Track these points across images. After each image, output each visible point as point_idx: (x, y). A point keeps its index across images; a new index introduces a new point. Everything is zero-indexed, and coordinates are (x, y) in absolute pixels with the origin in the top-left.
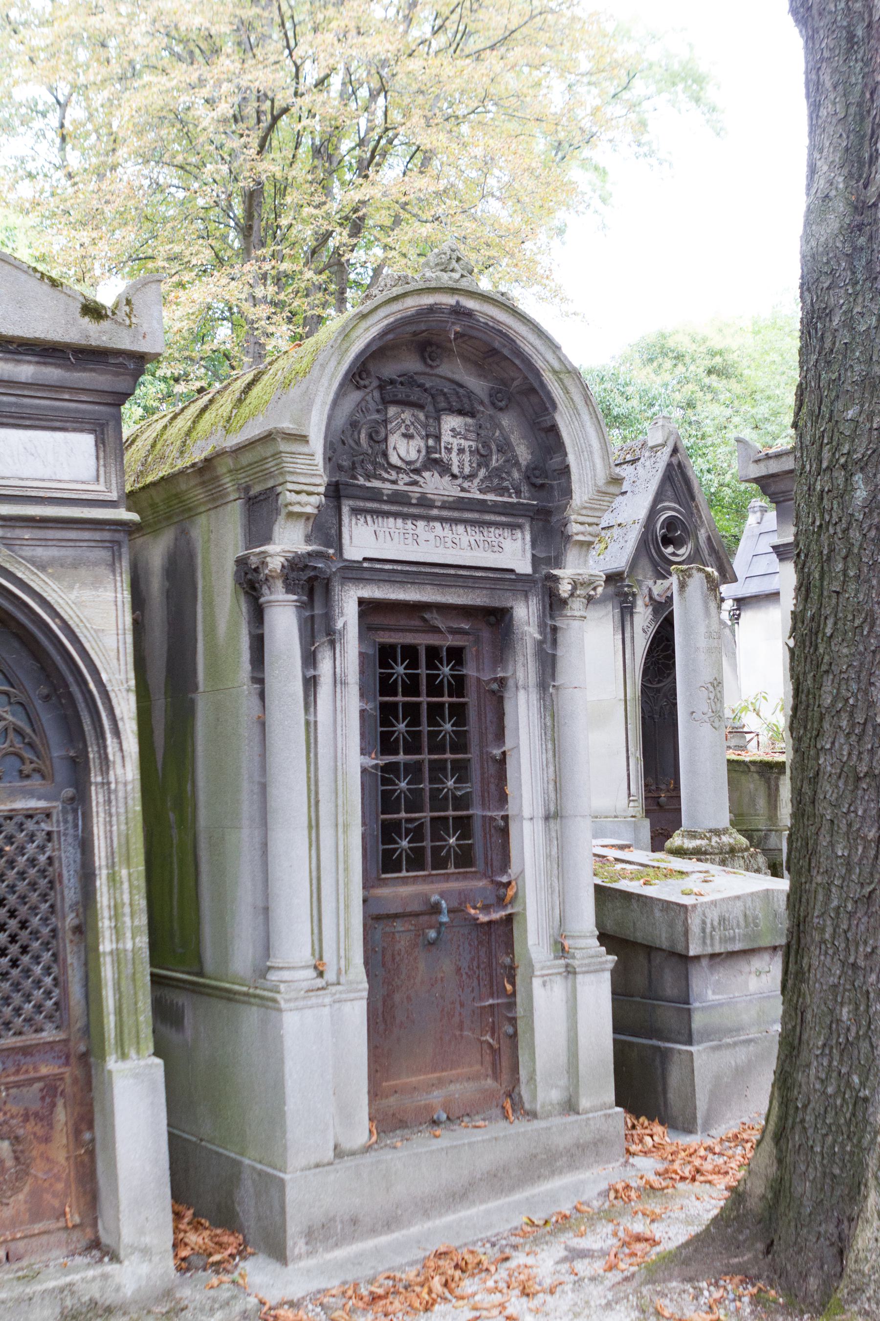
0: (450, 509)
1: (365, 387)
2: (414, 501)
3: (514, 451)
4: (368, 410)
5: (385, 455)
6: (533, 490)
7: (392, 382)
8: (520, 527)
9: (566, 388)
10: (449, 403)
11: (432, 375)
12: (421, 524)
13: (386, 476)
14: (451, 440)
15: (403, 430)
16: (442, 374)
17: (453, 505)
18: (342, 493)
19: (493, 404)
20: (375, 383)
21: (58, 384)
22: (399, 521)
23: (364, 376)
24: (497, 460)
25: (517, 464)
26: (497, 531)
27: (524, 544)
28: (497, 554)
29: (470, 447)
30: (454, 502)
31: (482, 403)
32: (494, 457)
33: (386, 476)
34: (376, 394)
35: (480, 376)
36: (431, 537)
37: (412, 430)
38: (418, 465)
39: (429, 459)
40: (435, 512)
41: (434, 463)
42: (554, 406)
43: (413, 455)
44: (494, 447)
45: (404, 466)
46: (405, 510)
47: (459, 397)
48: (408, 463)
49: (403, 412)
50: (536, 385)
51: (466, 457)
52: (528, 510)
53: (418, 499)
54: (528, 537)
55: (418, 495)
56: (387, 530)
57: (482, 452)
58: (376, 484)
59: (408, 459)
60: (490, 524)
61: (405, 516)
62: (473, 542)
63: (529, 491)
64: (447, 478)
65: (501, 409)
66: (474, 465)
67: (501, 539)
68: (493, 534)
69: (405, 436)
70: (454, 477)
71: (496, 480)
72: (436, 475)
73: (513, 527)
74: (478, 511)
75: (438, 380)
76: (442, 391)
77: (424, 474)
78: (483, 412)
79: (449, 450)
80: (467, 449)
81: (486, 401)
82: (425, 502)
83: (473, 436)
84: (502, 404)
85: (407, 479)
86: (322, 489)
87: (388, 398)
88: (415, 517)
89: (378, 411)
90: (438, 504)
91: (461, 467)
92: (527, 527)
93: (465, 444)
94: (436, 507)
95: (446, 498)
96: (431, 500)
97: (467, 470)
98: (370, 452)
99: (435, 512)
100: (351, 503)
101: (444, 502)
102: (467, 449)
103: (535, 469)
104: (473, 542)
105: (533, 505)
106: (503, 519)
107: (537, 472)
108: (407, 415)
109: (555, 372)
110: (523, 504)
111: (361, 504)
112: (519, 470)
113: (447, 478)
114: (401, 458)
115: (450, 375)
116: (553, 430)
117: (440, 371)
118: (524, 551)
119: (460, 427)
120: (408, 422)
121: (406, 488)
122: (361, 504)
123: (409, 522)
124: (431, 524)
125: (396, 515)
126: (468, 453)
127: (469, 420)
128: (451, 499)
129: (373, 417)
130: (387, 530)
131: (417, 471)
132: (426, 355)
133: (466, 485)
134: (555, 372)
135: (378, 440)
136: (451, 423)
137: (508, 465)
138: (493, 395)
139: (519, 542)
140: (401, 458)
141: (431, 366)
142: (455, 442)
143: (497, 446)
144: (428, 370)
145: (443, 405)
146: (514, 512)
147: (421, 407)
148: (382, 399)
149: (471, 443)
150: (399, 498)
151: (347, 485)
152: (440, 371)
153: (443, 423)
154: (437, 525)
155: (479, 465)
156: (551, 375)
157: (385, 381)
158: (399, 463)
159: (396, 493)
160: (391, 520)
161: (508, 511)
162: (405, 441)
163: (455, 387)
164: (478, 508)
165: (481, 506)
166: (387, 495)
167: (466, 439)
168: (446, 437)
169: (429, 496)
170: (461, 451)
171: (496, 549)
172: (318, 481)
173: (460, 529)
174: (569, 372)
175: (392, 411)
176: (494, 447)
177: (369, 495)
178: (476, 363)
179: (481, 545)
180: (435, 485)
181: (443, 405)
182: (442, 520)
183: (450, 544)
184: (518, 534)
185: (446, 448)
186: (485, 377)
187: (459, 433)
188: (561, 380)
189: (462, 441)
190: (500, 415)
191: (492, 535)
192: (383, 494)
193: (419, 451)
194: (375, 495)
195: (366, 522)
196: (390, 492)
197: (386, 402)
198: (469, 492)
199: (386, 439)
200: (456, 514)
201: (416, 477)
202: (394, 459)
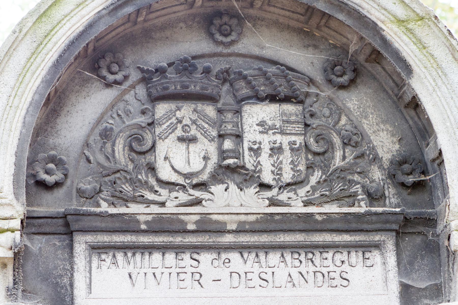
0: (253, 231)
1: (116, 83)
2: (191, 227)
3: (370, 142)
4: (128, 113)
5: (152, 169)
6: (405, 193)
7: (160, 71)
8: (377, 246)
9: (420, 41)
10: (253, 88)
11: (230, 55)
12: (206, 258)
13: (150, 196)
14: (259, 138)
15: (179, 132)
16: (243, 51)
17: (257, 227)
18: (74, 226)
19: (330, 81)
20: (135, 76)
21: (311, 233)
22: (170, 257)
23: (115, 68)
24: (344, 158)
25: (376, 159)
26: (338, 257)
27: (386, 271)
28: (339, 290)
29: (292, 143)
30: (257, 221)
31: (311, 82)
32: (338, 154)
33: (150, 196)
34: (141, 91)
35: (307, 47)
36: (224, 273)
37: (193, 131)
38: (205, 177)
39: (220, 166)
40: (228, 239)
41: (231, 171)
42: (408, 69)
43: (197, 164)
44: (337, 141)
45: (181, 181)
46: (178, 240)
47: (268, 79)
48: (187, 176)
49: (179, 109)
50: (377, 45)
51: (287, 157)
52: (387, 222)
53: (196, 222)
54: (392, 260)
55: (197, 218)
56: (151, 271)
57: (315, 147)
58: (134, 208)
59: (186, 170)
60: (324, 247)
61: (179, 249)
62: (296, 276)
63: (398, 194)
64: (252, 190)
65: (342, 87)
66: (302, 167)
67: (345, 267)
68: (330, 262)
69: (181, 139)
70: (264, 186)
71: (337, 185)
72: (233, 187)
73: (365, 248)
74: (301, 231)
75: (240, 61)
76: (240, 73)
77: (213, 189)
78: (317, 95)
79: (256, 152)
80: (286, 147)
81: (319, 78)
82: (207, 226)
83: (299, 128)
84: (344, 79)
85: (183, 197)
86: (16, 224)
87: (155, 93)
88: (196, 249)
89: (143, 112)
90: (234, 227)
91: (278, 171)
92: (390, 245)
93: (285, 140)
94: (229, 232)
95: (243, 218)
96: (217, 222)
97: (287, 177)
98: (131, 167)
99: (228, 239)
100: (90, 238)
101: (241, 223)
102: (286, 147)
103: (402, 163)
104: (296, 276)
105: (395, 214)
106: (347, 238)
107: (406, 167)
108: (186, 111)
109: (401, 22)
110: (376, 214)
111: (105, 238)
112: (381, 167)
113: (252, 190)
114: (176, 171)
115: (256, 51)
116: (415, 104)
117: (239, 48)
118: (386, 281)
119: (274, 119)
120: (187, 121)
121: (175, 210)
122: (105, 238)
123: (187, 256)
124: (224, 256)
125: (164, 249)
126: (287, 153)
127: (289, 108)
128: (252, 218)
129: (134, 121)
130: (151, 271)
131: (201, 186)
132: (214, 30)
133: (283, 197)
134: (401, 22)
135: (142, 149)
136: (257, 114)
137: (362, 163)
138: (330, 69)
139: (378, 268)
140: (176, 171)
141: (222, 43)
142: (266, 141)
143: (343, 138)
144: (220, 49)
145: (245, 91)
146: (365, 226)
147: (211, 99)
148: (149, 95)
149: (293, 138)
150: (164, 226)
151: (78, 214)
152: (239, 48)
153: (245, 116)
154: (235, 256)
155: (310, 167)
156: (395, 27)
157: (148, 71)
158: (174, 178)
159: (159, 218)
160: (157, 256)
161: (354, 226)
162: (183, 146)
163: (261, 65)
164: (301, 226)
165: (307, 223)
166: (146, 222)
167: (282, 133)
168: (251, 134)
169: (215, 217)
170: (276, 150)
171: (338, 281)
172: (7, 212)
173: (274, 258)
174: (422, 19)
175: (162, 109)
176: (337, 141)
177: (117, 225)
178: (300, 32)
179: (310, 278)
180: (231, 202)
181: (245, 91)
182: (241, 249)
183: (257, 281)
184: (375, 257)
185: (251, 149)
186: (316, 47)
187: (273, 127)
188: (410, 31)
189: (278, 138)
190: (343, 94)
191: (329, 262)
192: (138, 222)
193: (206, 158)
194: (128, 225)
195: (115, 263)
196: (150, 218)
197: (155, 99)
198: (288, 205)
199: (153, 147)
200: (265, 239)
201: (197, 194)
202: (165, 173)
